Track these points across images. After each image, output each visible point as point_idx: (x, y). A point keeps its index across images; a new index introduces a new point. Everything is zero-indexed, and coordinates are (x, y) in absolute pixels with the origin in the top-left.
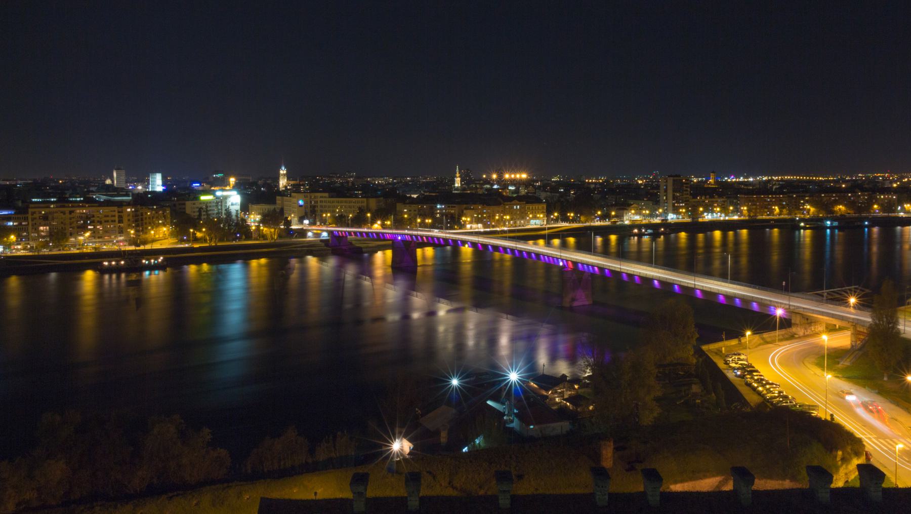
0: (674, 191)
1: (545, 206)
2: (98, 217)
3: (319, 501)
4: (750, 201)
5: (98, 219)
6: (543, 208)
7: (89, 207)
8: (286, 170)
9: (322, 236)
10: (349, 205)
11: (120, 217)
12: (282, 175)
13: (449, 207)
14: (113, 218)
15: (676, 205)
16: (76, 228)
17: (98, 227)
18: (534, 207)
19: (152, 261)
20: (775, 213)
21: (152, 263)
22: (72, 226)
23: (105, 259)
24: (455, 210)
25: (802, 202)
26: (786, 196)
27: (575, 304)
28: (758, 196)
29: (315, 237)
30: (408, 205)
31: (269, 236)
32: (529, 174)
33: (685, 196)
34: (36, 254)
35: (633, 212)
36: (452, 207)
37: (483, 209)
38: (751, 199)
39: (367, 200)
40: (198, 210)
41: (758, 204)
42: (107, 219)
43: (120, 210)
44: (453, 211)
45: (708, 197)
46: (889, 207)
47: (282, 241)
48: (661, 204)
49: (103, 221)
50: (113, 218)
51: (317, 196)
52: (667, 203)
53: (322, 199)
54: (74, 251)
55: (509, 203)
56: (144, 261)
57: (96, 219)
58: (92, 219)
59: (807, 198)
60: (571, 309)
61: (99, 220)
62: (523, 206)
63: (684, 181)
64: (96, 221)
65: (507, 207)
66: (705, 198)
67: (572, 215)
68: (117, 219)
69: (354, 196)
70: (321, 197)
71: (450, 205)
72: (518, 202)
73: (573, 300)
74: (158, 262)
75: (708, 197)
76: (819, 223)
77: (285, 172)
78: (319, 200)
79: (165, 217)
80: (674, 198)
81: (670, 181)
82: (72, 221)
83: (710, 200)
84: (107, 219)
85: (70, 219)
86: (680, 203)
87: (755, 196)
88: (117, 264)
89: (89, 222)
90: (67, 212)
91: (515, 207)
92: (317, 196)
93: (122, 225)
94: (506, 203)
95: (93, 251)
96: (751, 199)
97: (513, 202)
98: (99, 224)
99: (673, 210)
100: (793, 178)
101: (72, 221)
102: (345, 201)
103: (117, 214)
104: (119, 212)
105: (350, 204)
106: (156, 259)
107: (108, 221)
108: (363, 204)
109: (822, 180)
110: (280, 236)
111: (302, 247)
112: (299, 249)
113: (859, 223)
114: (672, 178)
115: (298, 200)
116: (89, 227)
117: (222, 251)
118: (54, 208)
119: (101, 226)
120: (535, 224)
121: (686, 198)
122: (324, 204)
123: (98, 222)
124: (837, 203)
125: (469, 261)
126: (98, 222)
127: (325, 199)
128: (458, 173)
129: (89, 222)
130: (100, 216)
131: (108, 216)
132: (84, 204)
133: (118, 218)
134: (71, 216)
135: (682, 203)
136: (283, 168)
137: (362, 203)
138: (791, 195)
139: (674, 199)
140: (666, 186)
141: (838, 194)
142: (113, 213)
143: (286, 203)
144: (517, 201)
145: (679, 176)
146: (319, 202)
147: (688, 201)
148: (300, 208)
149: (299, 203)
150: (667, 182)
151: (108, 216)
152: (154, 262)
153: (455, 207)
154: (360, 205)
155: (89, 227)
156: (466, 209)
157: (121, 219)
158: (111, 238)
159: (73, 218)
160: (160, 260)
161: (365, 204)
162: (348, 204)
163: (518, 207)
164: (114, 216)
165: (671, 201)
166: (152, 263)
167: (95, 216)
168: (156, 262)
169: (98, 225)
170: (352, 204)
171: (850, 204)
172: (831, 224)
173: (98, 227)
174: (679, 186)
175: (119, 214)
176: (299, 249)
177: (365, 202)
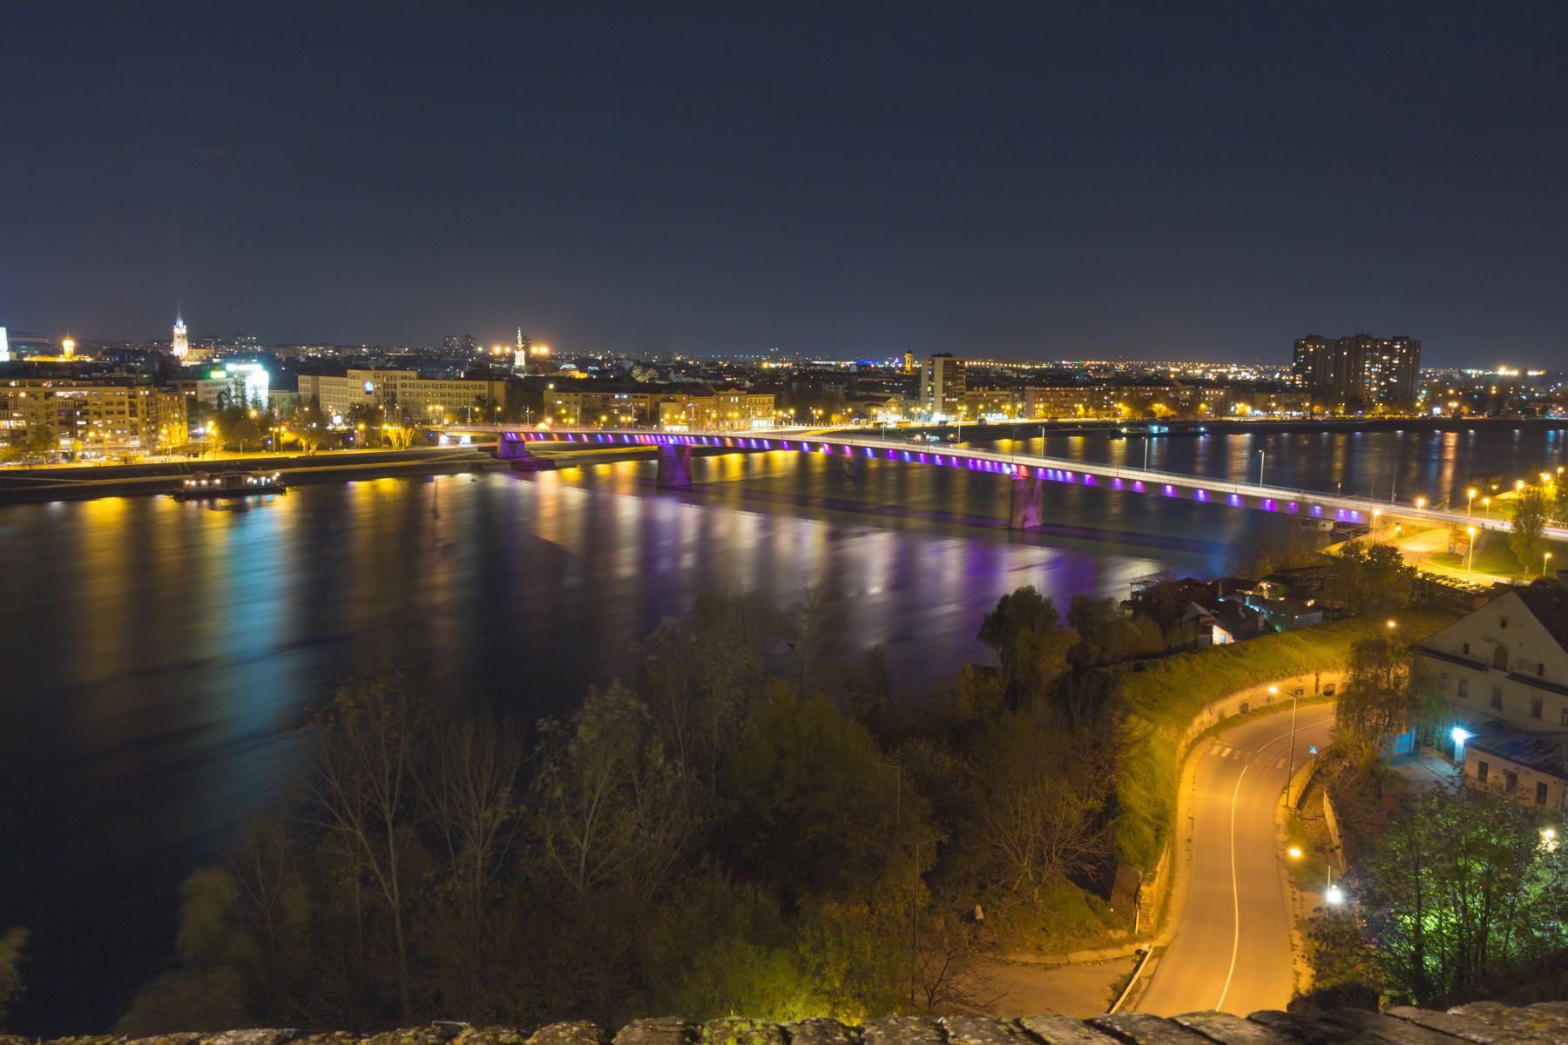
0: (946, 378)
1: (773, 398)
2: (95, 405)
3: (15, 1034)
4: (1042, 396)
5: (95, 408)
6: (770, 401)
7: (77, 386)
8: (187, 329)
9: (462, 442)
10: (457, 391)
11: (132, 405)
12: (178, 337)
13: (636, 397)
14: (121, 408)
15: (947, 399)
16: (57, 424)
17: (95, 423)
18: (757, 399)
19: (263, 479)
20: (1078, 413)
21: (263, 484)
22: (50, 420)
23: (187, 476)
24: (646, 403)
25: (1106, 398)
26: (1087, 389)
27: (1028, 525)
28: (1053, 389)
29: (452, 444)
30: (564, 394)
31: (394, 440)
32: (552, 345)
33: (959, 387)
34: (27, 468)
35: (894, 409)
36: (642, 397)
37: (689, 401)
38: (1044, 393)
39: (489, 384)
40: (215, 395)
41: (1052, 400)
42: (110, 408)
43: (132, 393)
44: (642, 405)
45: (987, 388)
46: (1221, 407)
47: (417, 449)
48: (921, 398)
49: (103, 413)
50: (121, 408)
51: (395, 377)
52: (932, 396)
53: (404, 381)
54: (64, 464)
55: (724, 393)
56: (250, 480)
57: (91, 408)
58: (85, 408)
59: (1112, 393)
60: (1023, 530)
61: (97, 410)
62: (743, 398)
63: (958, 363)
64: (91, 413)
65: (722, 399)
66: (984, 390)
67: (820, 412)
68: (126, 408)
69: (113, 383)
70: (402, 378)
71: (639, 395)
72: (738, 392)
73: (1025, 519)
74: (271, 480)
75: (987, 388)
76: (1141, 429)
77: (184, 331)
78: (399, 382)
79: (180, 407)
80: (946, 389)
81: (940, 362)
82: (49, 411)
83: (990, 393)
84: (110, 408)
85: (47, 407)
86: (952, 397)
87: (1048, 389)
88: (210, 484)
89: (78, 413)
90: (41, 395)
91: (732, 399)
92: (395, 377)
93: (134, 419)
94: (720, 392)
95: (123, 464)
96: (1044, 393)
97: (730, 392)
98: (96, 416)
99: (943, 407)
100: (986, 365)
101: (49, 411)
102: (456, 386)
103: (127, 400)
104: (130, 397)
105: (459, 391)
106: (268, 476)
107: (112, 413)
108: (482, 391)
109: (770, 369)
110: (414, 443)
111: (460, 459)
112: (458, 462)
113: (1193, 429)
114: (942, 359)
115: (364, 383)
116: (79, 423)
117: (105, 478)
118: (16, 386)
119: (101, 421)
120: (759, 428)
121: (960, 389)
122: (408, 390)
123: (95, 413)
124: (1155, 399)
125: (366, 516)
126: (95, 413)
127: (411, 381)
128: (520, 342)
129: (78, 413)
130: (99, 403)
131: (111, 404)
132: (69, 381)
133: (130, 407)
134: (48, 402)
135: (955, 397)
136: (180, 323)
137: (480, 388)
138: (1092, 387)
139: (944, 391)
140: (933, 371)
141: (1153, 388)
142: (121, 399)
143: (325, 387)
144: (735, 390)
145: (950, 356)
146: (398, 386)
147: (963, 394)
148: (368, 395)
149: (366, 389)
150: (933, 364)
151: (111, 404)
152: (266, 481)
153: (646, 397)
154: (477, 392)
155: (79, 423)
156: (665, 400)
157: (133, 409)
158: (118, 443)
159: (52, 405)
160: (274, 478)
161: (485, 391)
162: (440, 391)
163: (737, 399)
164: (122, 403)
165: (940, 394)
166: (263, 484)
167: (89, 402)
168: (269, 481)
169: (96, 420)
170: (446, 391)
171: (1173, 403)
172: (1159, 430)
173: (95, 423)
174: (952, 372)
175: (131, 400)
176: (458, 462)
177: (487, 387)
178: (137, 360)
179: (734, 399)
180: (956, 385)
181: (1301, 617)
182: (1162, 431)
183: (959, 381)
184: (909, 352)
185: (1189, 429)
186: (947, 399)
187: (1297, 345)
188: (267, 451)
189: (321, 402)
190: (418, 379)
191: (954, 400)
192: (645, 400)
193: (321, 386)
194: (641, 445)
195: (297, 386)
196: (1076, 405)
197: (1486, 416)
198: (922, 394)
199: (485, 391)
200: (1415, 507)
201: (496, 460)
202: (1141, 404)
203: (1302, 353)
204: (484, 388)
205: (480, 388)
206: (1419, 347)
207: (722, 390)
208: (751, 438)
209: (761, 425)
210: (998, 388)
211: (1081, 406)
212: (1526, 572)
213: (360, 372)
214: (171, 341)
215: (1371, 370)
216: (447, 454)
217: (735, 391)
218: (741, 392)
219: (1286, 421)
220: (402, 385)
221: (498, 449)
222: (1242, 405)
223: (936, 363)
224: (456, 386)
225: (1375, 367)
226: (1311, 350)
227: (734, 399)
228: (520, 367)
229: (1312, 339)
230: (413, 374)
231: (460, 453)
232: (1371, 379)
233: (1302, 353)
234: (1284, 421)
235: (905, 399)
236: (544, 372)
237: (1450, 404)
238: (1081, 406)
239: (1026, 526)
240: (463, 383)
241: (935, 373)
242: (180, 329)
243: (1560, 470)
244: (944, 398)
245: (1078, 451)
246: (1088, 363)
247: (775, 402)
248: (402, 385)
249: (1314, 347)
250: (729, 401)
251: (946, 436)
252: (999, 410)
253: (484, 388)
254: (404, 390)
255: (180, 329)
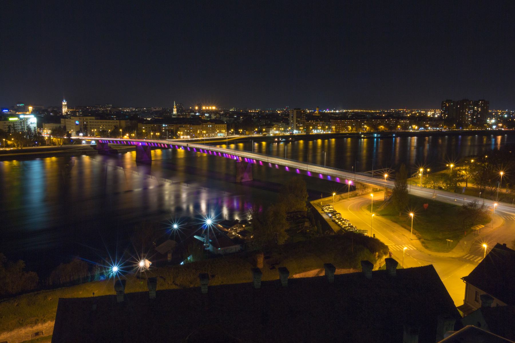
0: (297, 117)
4: (336, 123)
8: (67, 103)
9: (92, 143)
12: (64, 105)
13: (170, 126)
15: (298, 125)
25: (363, 124)
27: (243, 180)
28: (341, 121)
31: (57, 143)
32: (216, 107)
36: (172, 126)
39: (119, 121)
40: (8, 127)
45: (315, 121)
46: (405, 127)
52: (293, 124)
55: (205, 124)
59: (365, 122)
60: (241, 183)
62: (213, 125)
63: (302, 112)
65: (204, 126)
67: (241, 130)
70: (90, 119)
71: (171, 125)
72: (211, 123)
73: (242, 178)
75: (315, 121)
76: (371, 135)
77: (66, 103)
80: (297, 121)
83: (316, 122)
86: (300, 124)
87: (339, 121)
91: (209, 126)
94: (203, 124)
96: (337, 122)
97: (208, 123)
102: (100, 122)
108: (117, 124)
111: (79, 150)
114: (296, 110)
115: (75, 121)
121: (303, 121)
122: (92, 123)
124: (380, 124)
128: (175, 106)
135: (301, 124)
137: (116, 123)
139: (297, 122)
141: (381, 120)
146: (89, 122)
147: (304, 123)
148: (77, 126)
150: (293, 112)
153: (173, 126)
161: (118, 124)
162: (108, 124)
163: (211, 126)
165: (295, 123)
170: (110, 124)
171: (386, 125)
172: (377, 136)
177: (119, 122)
178: (44, 113)
179: (210, 126)
180: (301, 120)
181: (223, 249)
182: (378, 136)
183: (303, 118)
184: (318, 107)
185: (389, 135)
186: (298, 125)
187: (443, 103)
188: (244, 135)
189: (67, 128)
190: (95, 119)
191: (301, 125)
192: (173, 126)
193: (67, 123)
194: (132, 145)
195: (60, 122)
196: (348, 127)
197: (513, 129)
198: (290, 123)
199: (118, 124)
200: (384, 179)
201: (95, 150)
202: (375, 127)
203: (444, 106)
204: (118, 123)
205: (116, 123)
206: (489, 103)
207: (204, 123)
208: (171, 145)
209: (221, 135)
210: (319, 121)
211: (350, 127)
212: (400, 215)
213: (74, 117)
214: (62, 108)
215: (468, 113)
216: (79, 148)
217: (210, 123)
218: (212, 123)
219: (431, 132)
220: (90, 122)
221: (97, 146)
222: (415, 126)
223: (294, 112)
224: (113, 122)
225: (470, 111)
226: (447, 105)
227: (210, 126)
228: (175, 114)
229: (448, 101)
230: (94, 118)
231: (82, 147)
232: (468, 115)
233: (444, 106)
234: (430, 132)
235: (285, 125)
236: (182, 116)
237: (499, 125)
238: (350, 127)
239: (242, 181)
240: (115, 121)
241: (294, 115)
242: (64, 103)
243: (447, 165)
244: (297, 125)
245: (264, 149)
246: (401, 109)
247: (227, 127)
248: (90, 122)
249: (449, 104)
250: (208, 126)
251: (288, 139)
252: (317, 129)
253: (118, 123)
254: (91, 123)
255: (64, 103)
